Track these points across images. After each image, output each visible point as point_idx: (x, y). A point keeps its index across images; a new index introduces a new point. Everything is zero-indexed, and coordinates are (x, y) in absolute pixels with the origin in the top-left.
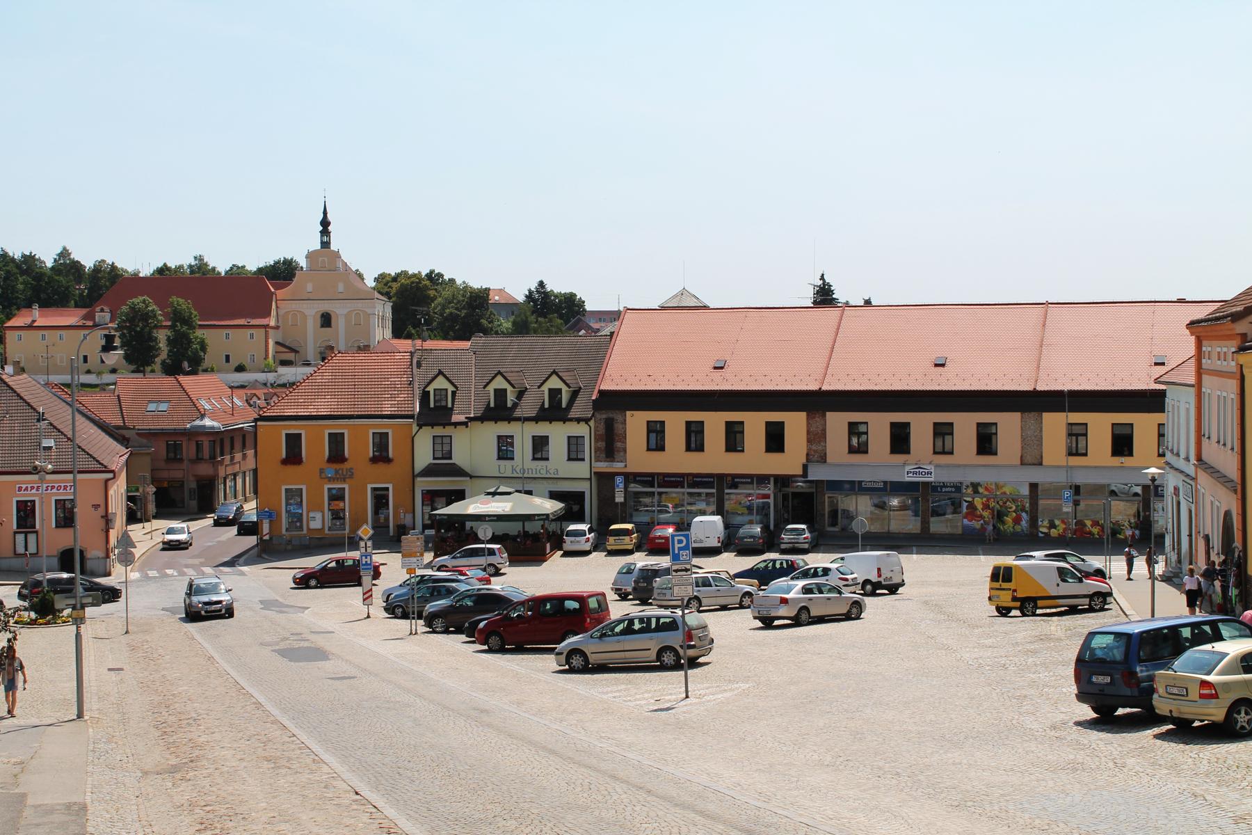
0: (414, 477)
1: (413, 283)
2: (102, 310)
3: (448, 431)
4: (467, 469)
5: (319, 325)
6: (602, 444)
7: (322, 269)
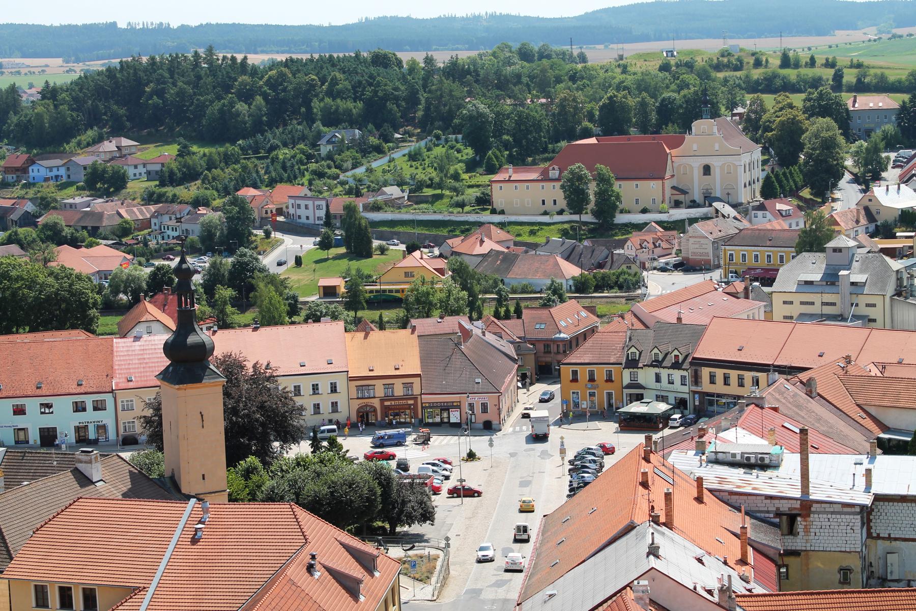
1: (789, 119)
2: (554, 169)
3: (635, 370)
4: (644, 385)
5: (702, 173)
6: (693, 379)
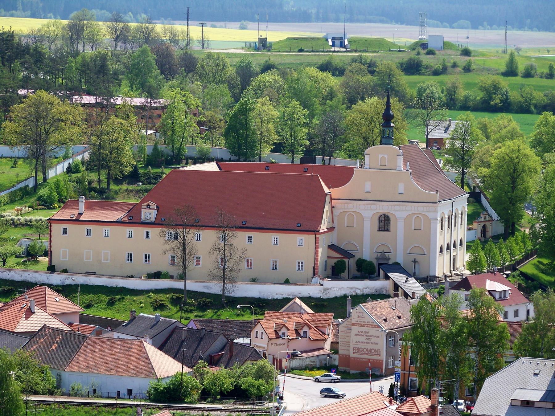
0: (180, 322)
2: (149, 207)
7: (382, 167)
